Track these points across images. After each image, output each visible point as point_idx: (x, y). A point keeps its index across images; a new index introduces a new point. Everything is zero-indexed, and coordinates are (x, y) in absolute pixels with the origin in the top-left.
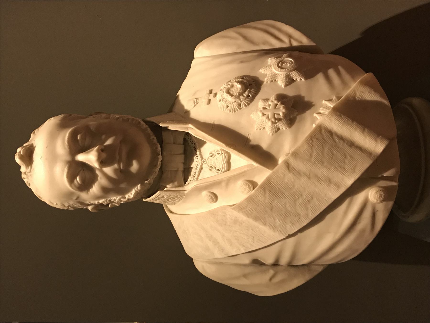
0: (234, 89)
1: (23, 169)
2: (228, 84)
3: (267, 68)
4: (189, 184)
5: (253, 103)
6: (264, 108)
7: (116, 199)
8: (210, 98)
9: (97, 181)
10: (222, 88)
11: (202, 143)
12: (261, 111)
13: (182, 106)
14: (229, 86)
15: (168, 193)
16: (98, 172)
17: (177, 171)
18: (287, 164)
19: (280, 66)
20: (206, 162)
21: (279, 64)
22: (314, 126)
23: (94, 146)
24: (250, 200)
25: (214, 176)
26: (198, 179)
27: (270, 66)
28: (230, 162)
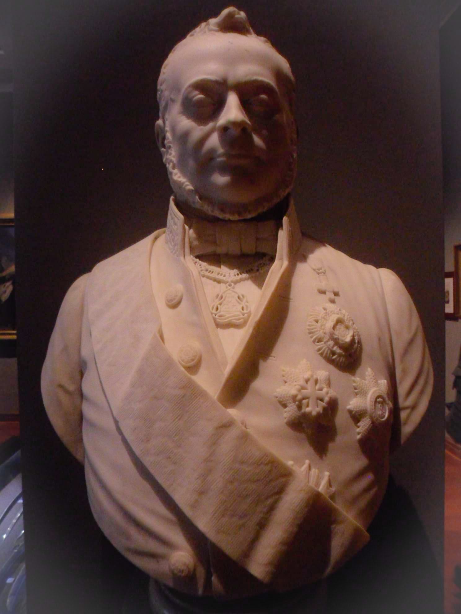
0: (343, 331)
1: (213, 21)
2: (349, 321)
3: (374, 379)
4: (196, 263)
5: (323, 361)
6: (316, 381)
7: (172, 155)
8: (327, 293)
9: (197, 124)
10: (344, 311)
11: (259, 281)
12: (312, 376)
13: (312, 251)
14: (347, 323)
15: (180, 230)
16: (211, 125)
17: (214, 243)
18: (228, 425)
19: (378, 400)
20: (229, 289)
21: (380, 398)
22: (290, 463)
23: (250, 118)
24: (169, 363)
25: (81, 328)
26: (204, 276)
27: (376, 384)
28: (235, 32)
